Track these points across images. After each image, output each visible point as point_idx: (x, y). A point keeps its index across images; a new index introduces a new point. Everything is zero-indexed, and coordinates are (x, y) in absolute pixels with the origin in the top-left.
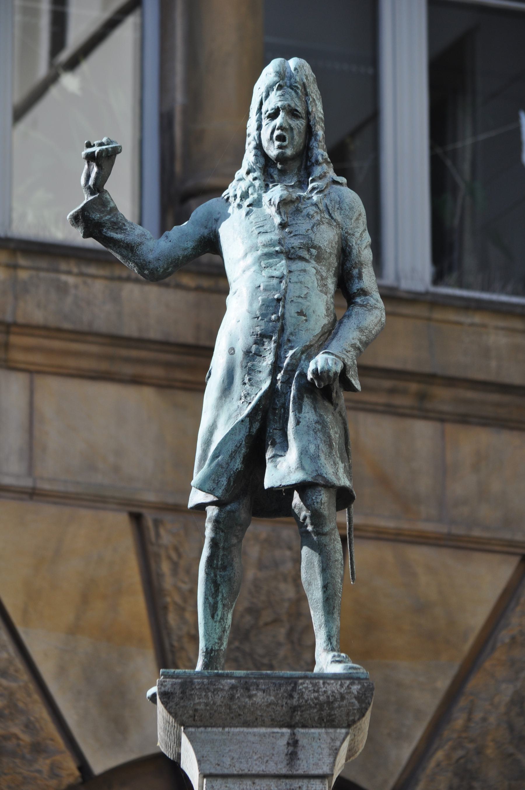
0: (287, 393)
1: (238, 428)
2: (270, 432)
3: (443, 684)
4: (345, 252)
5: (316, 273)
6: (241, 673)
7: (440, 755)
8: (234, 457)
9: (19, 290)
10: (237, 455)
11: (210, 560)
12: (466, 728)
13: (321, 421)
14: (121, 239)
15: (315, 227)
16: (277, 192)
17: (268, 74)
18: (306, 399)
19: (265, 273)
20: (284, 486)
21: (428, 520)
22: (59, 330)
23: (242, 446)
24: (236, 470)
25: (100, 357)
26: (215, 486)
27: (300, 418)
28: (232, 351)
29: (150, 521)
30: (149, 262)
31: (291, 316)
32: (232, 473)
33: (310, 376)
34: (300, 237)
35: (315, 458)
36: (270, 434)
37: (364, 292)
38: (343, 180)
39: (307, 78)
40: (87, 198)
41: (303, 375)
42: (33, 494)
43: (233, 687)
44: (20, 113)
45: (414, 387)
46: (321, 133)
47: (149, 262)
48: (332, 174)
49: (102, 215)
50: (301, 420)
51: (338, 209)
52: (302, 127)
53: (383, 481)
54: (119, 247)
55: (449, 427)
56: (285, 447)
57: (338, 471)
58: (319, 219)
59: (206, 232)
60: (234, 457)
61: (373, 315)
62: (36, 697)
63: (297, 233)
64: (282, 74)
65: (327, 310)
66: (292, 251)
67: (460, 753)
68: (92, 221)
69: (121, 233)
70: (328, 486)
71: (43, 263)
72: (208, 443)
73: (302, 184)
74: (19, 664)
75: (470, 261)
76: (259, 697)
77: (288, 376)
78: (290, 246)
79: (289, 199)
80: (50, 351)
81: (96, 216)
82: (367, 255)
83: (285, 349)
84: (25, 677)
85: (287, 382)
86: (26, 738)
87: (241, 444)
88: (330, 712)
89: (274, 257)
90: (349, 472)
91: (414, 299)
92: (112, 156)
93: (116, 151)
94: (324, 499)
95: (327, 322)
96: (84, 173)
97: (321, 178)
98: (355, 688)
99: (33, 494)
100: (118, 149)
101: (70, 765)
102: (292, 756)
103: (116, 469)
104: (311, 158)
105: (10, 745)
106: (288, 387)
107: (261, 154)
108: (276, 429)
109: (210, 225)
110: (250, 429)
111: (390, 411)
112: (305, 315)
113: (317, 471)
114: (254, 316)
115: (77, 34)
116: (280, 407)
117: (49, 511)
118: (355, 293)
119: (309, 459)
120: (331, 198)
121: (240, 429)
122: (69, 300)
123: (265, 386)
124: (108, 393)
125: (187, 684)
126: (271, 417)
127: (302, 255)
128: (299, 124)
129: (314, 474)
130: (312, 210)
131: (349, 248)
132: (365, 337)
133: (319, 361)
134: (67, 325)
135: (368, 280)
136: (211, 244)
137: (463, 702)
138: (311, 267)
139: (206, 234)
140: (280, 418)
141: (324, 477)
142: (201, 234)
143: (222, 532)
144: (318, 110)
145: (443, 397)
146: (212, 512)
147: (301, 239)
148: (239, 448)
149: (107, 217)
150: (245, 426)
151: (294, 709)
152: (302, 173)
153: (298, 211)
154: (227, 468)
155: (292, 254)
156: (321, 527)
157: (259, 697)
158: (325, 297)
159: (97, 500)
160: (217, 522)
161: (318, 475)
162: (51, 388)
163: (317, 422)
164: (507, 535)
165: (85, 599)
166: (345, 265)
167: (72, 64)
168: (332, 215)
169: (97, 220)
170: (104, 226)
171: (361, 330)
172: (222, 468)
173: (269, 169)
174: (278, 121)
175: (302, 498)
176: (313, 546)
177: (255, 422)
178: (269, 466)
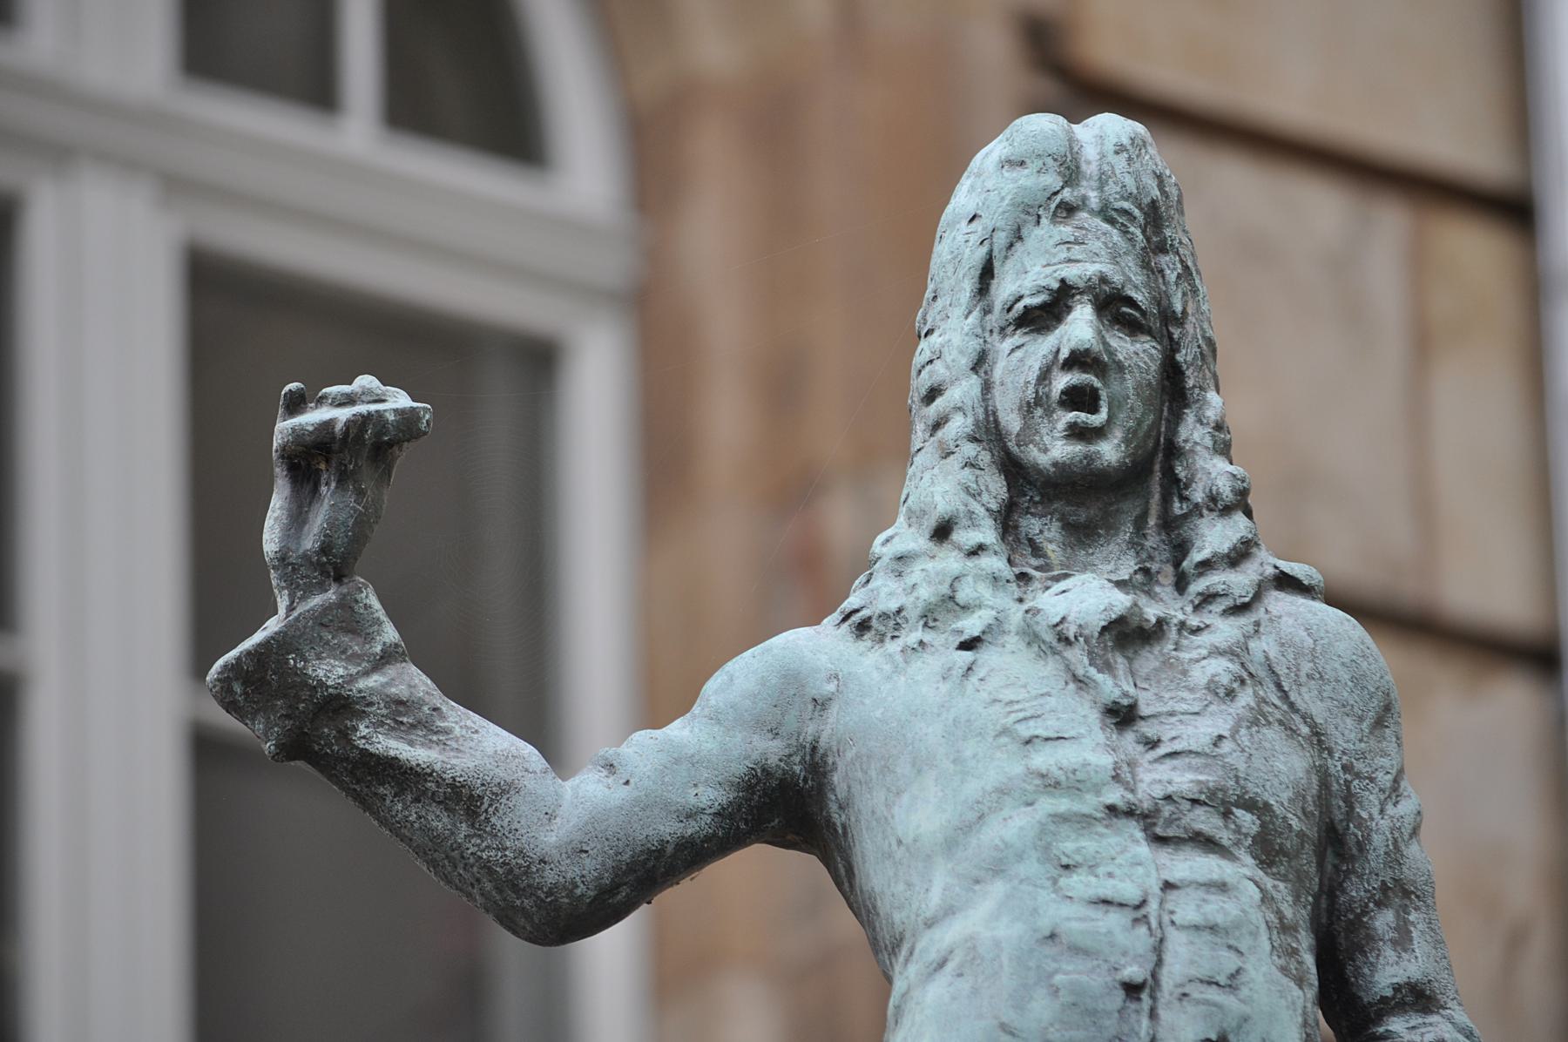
5: (1262, 900)
15: (1243, 731)
30: (542, 861)
34: (1196, 761)
39: (1161, 185)
47: (542, 861)
52: (1153, 368)
54: (417, 800)
58: (1253, 704)
59: (771, 750)
63: (1177, 746)
66: (1167, 810)
69: (429, 744)
78: (1158, 792)
89: (1101, 829)
92: (390, 444)
100: (419, 419)
104: (1187, 486)
109: (790, 723)
118: (1384, 999)
120: (1278, 633)
131: (1359, 827)
139: (773, 761)
142: (755, 756)
147: (1197, 770)
149: (374, 681)
152: (1151, 542)
155: (1169, 822)
158: (1297, 992)
166: (1344, 891)
168: (1293, 696)
170: (362, 715)
173: (1023, 522)
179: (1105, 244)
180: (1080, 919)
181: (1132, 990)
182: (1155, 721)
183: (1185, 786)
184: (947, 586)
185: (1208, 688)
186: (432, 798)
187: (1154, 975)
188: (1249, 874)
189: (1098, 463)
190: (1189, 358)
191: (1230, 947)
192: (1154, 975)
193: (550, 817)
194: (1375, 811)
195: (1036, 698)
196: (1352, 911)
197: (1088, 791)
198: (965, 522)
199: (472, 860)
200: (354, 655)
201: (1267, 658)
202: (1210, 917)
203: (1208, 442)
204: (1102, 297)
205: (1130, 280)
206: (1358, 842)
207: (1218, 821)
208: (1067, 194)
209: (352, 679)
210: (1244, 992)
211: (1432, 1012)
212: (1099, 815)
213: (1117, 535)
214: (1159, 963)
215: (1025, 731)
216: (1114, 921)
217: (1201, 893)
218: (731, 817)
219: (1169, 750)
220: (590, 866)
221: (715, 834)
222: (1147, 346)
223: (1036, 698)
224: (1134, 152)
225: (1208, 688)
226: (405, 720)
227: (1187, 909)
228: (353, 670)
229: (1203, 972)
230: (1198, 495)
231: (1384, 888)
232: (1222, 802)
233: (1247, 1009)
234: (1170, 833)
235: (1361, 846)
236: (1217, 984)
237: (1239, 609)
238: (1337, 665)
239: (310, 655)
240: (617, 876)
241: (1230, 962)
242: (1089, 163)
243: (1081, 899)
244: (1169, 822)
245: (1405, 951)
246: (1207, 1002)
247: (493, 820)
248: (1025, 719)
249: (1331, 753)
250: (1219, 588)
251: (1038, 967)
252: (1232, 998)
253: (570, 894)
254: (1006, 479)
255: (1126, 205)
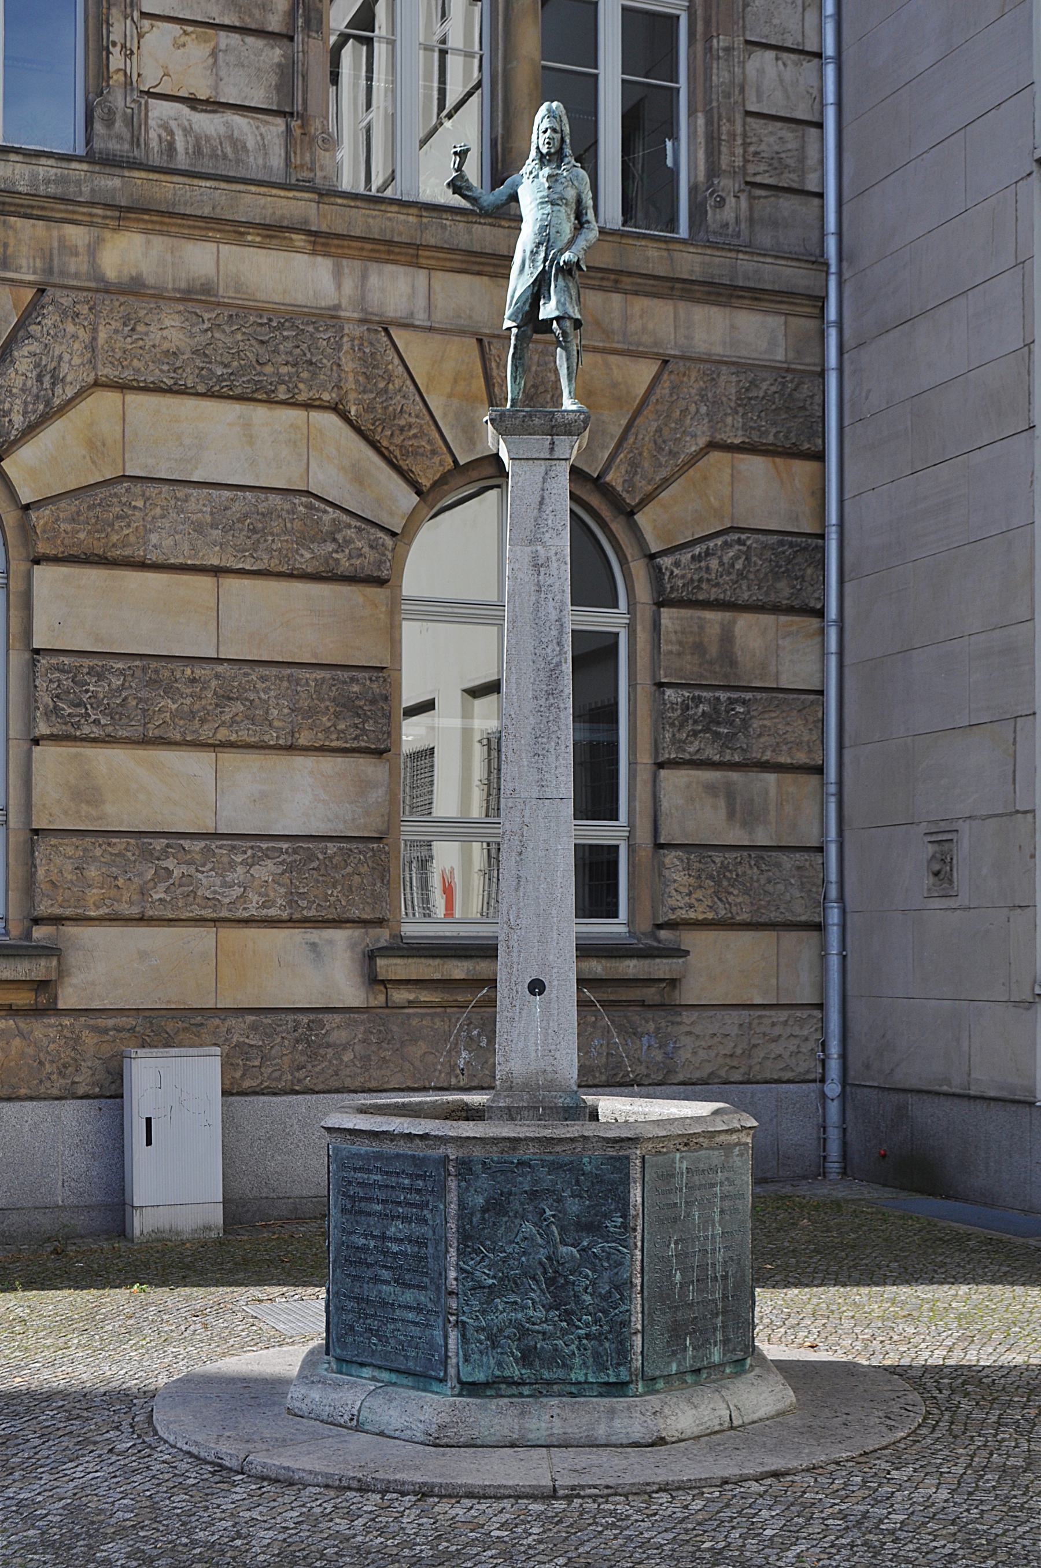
3: (624, 422)
4: (579, 201)
6: (528, 409)
7: (622, 455)
9: (423, 228)
11: (514, 354)
12: (634, 443)
16: (546, 171)
17: (543, 110)
19: (541, 212)
21: (618, 342)
22: (442, 248)
25: (461, 261)
28: (524, 251)
29: (486, 343)
33: (562, 264)
35: (564, 304)
37: (588, 222)
38: (579, 165)
40: (455, 174)
41: (558, 263)
42: (431, 329)
43: (524, 416)
44: (424, 142)
45: (613, 277)
46: (568, 141)
48: (573, 161)
53: (597, 323)
55: (629, 296)
56: (549, 299)
61: (592, 234)
62: (433, 427)
64: (549, 110)
67: (632, 455)
70: (570, 318)
71: (434, 214)
72: (513, 297)
73: (559, 167)
74: (424, 411)
75: (640, 215)
76: (537, 421)
80: (439, 259)
82: (590, 203)
84: (428, 418)
85: (551, 267)
86: (428, 447)
88: (569, 428)
90: (580, 311)
91: (613, 233)
93: (468, 150)
94: (568, 324)
96: (453, 161)
97: (568, 163)
98: (582, 417)
99: (431, 329)
101: (450, 460)
102: (552, 450)
103: (470, 317)
105: (421, 450)
111: (601, 288)
115: (450, 102)
117: (438, 337)
122: (447, 233)
123: (540, 268)
124: (465, 280)
125: (502, 415)
128: (559, 136)
130: (563, 180)
133: (566, 256)
134: (446, 246)
135: (590, 215)
136: (514, 198)
137: (633, 430)
138: (563, 209)
144: (567, 129)
145: (627, 282)
146: (515, 331)
151: (553, 427)
153: (557, 180)
157: (537, 421)
159: (461, 332)
160: (517, 336)
162: (439, 276)
164: (656, 350)
165: (455, 381)
167: (450, 116)
171: (587, 241)
174: (547, 134)
175: (558, 324)
176: (562, 347)
178: (542, 308)
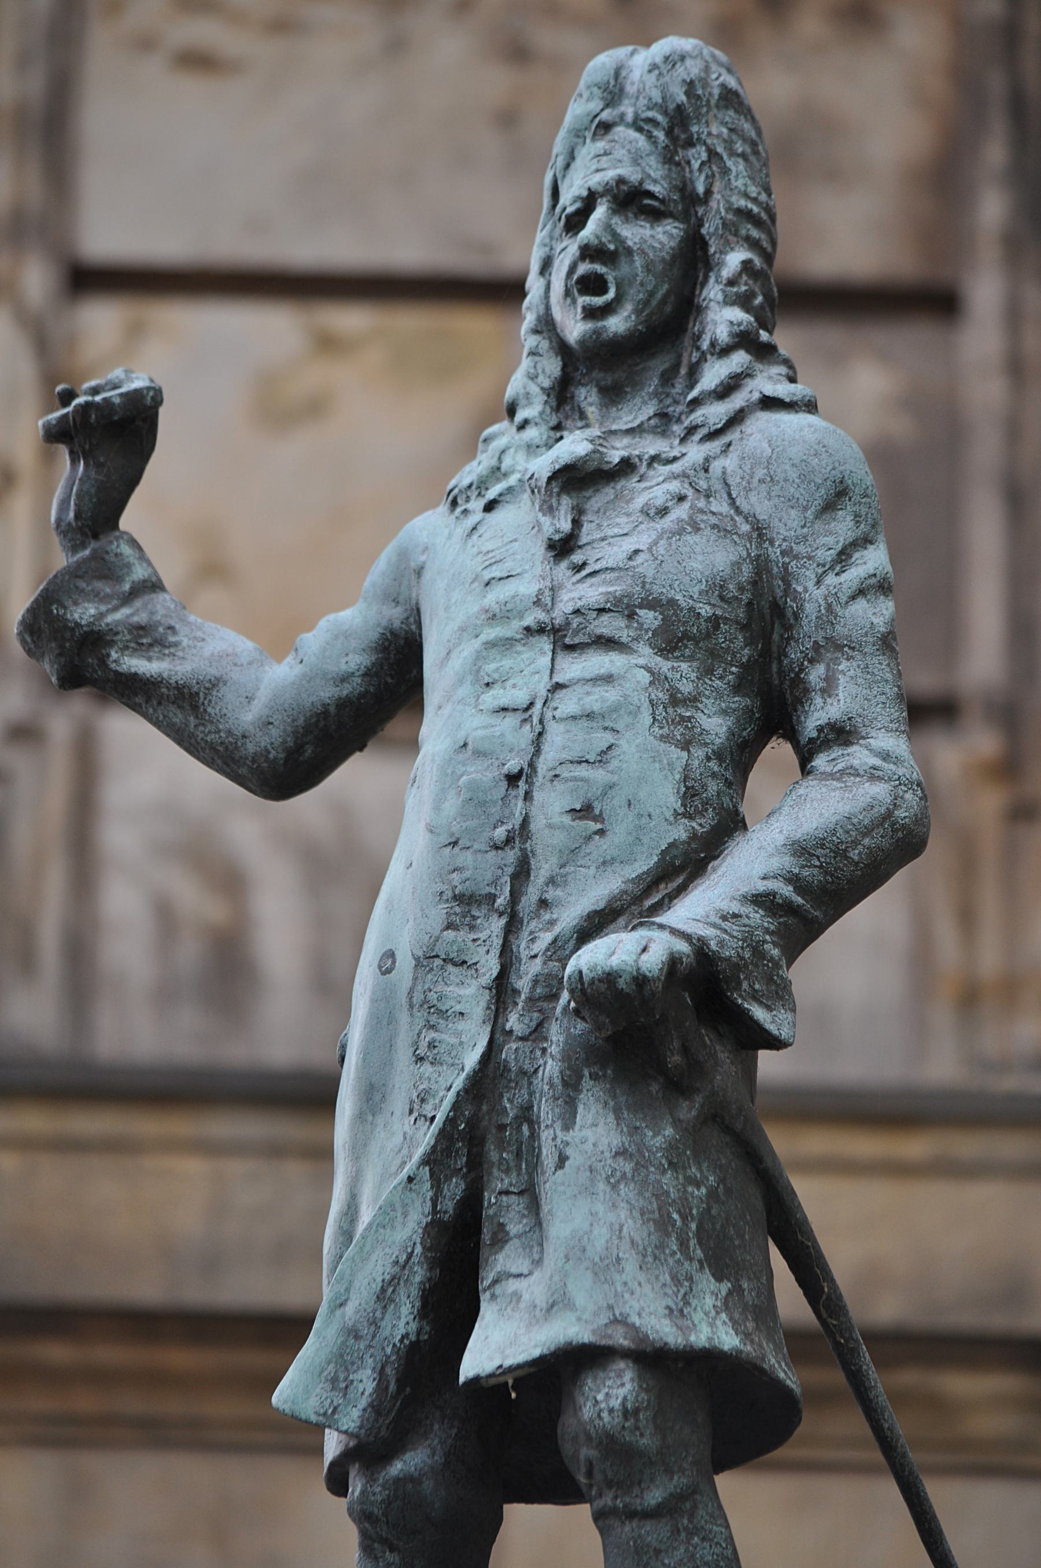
0: (536, 1071)
1: (398, 1205)
2: (490, 1205)
5: (651, 683)
8: (391, 1300)
10: (402, 1291)
13: (632, 1149)
14: (160, 675)
18: (587, 1083)
20: (511, 1369)
23: (415, 1259)
24: (401, 1341)
26: (338, 1400)
27: (568, 1144)
30: (244, 736)
31: (550, 826)
32: (389, 1350)
34: (609, 576)
36: (491, 1212)
47: (244, 736)
49: (103, 608)
50: (569, 1151)
51: (761, 481)
54: (160, 703)
57: (687, 1303)
60: (391, 1300)
63: (597, 567)
65: (684, 797)
66: (575, 622)
68: (73, 629)
69: (162, 657)
77: (536, 1015)
79: (593, 465)
81: (84, 612)
83: (532, 933)
87: (410, 1256)
95: (684, 836)
106: (538, 1053)
107: (551, 348)
108: (507, 1193)
110: (434, 1202)
112: (598, 818)
113: (611, 1307)
114: (445, 839)
116: (516, 1117)
118: (811, 740)
119: (589, 1274)
121: (404, 1206)
126: (494, 1155)
127: (605, 631)
129: (603, 1319)
131: (794, 600)
132: (816, 871)
139: (397, 624)
140: (518, 1154)
141: (633, 1325)
142: (384, 623)
143: (392, 1551)
147: (610, 583)
148: (404, 1267)
149: (122, 614)
150: (418, 1194)
154: (374, 1336)
156: (636, 1491)
161: (615, 1321)
163: (621, 1153)
166: (786, 656)
169: (88, 625)
170: (112, 643)
172: (357, 1337)
177: (448, 1179)
179: (629, 151)
180: (485, 727)
181: (512, 779)
182: (589, 547)
183: (593, 600)
184: (496, 459)
185: (642, 511)
186: (168, 700)
187: (532, 765)
188: (641, 661)
189: (604, 335)
190: (712, 230)
191: (606, 728)
192: (532, 765)
193: (249, 699)
194: (811, 585)
195: (506, 544)
196: (793, 670)
197: (514, 618)
198: (523, 402)
199: (203, 744)
200: (107, 596)
201: (724, 473)
202: (588, 707)
203: (720, 297)
204: (622, 196)
205: (649, 176)
206: (794, 613)
207: (621, 622)
208: (605, 115)
209: (102, 615)
210: (614, 764)
211: (852, 744)
212: (518, 637)
213: (642, 389)
214: (538, 752)
215: (487, 576)
216: (511, 721)
217: (588, 688)
218: (376, 674)
219: (591, 570)
220: (275, 734)
221: (367, 692)
222: (668, 228)
223: (506, 544)
224: (664, 69)
225: (642, 511)
226: (144, 641)
227: (568, 704)
228: (103, 608)
229: (573, 755)
230: (705, 345)
231: (817, 646)
232: (625, 607)
233: (615, 778)
234: (576, 641)
235: (796, 616)
236: (587, 761)
237: (713, 435)
238: (787, 467)
239: (68, 603)
240: (297, 738)
241: (603, 739)
242: (633, 84)
243: (488, 710)
244: (576, 632)
245: (830, 697)
246: (575, 779)
247: (209, 710)
248: (490, 565)
249: (772, 542)
250: (699, 421)
251: (453, 772)
252: (601, 771)
253: (267, 760)
254: (563, 359)
255: (650, 114)
